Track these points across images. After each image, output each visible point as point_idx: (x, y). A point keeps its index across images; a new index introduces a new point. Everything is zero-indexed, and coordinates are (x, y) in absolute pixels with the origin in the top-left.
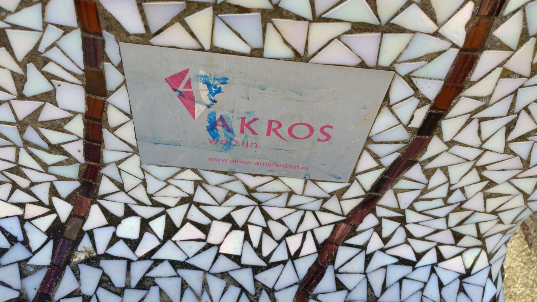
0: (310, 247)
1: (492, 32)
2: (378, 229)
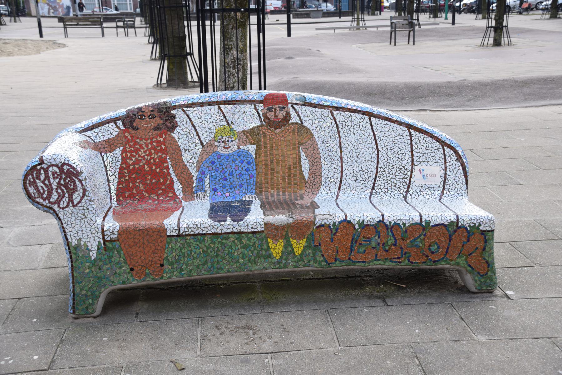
0: (438, 197)
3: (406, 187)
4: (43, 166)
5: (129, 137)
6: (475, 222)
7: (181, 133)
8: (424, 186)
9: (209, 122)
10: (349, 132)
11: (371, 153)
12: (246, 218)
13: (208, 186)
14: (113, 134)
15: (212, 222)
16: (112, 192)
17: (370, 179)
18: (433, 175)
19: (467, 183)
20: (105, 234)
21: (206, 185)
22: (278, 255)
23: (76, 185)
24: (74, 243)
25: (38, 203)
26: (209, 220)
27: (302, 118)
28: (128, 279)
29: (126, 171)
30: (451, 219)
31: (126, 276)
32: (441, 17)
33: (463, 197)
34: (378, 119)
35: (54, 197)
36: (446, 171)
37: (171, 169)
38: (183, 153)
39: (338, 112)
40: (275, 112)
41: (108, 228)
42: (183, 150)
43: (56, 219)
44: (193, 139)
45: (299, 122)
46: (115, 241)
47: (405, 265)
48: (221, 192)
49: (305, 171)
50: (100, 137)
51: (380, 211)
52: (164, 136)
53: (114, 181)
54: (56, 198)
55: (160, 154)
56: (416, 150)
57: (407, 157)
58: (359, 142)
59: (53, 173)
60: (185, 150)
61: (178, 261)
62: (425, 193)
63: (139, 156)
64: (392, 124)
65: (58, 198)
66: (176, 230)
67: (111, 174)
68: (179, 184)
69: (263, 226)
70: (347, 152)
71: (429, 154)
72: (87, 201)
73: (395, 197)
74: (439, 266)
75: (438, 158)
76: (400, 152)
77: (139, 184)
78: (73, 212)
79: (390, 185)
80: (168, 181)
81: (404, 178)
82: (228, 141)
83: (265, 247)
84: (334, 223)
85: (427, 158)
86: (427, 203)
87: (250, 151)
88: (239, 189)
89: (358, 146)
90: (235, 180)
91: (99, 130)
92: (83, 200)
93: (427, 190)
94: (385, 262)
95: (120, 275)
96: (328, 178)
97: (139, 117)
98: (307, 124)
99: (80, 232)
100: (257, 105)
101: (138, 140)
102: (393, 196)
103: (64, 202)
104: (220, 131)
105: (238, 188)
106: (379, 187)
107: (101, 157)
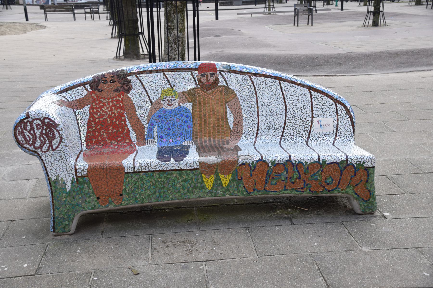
0: (332, 141)
2: (338, 139)
3: (308, 134)
4: (29, 119)
5: (95, 97)
6: (360, 160)
7: (135, 93)
8: (321, 133)
11: (281, 108)
12: (185, 158)
13: (156, 134)
14: (83, 95)
15: (159, 162)
16: (82, 139)
17: (280, 128)
18: (328, 125)
19: (354, 131)
20: (78, 171)
22: (210, 187)
23: (55, 134)
24: (54, 178)
25: (25, 148)
26: (157, 160)
27: (228, 82)
28: (95, 206)
29: (93, 123)
30: (342, 159)
32: (333, 4)
33: (351, 142)
34: (286, 83)
35: (38, 143)
37: (128, 122)
38: (136, 109)
39: (255, 77)
40: (207, 78)
41: (80, 167)
42: (137, 107)
44: (144, 98)
45: (226, 85)
46: (85, 176)
47: (307, 194)
48: (166, 138)
49: (230, 122)
50: (72, 97)
51: (288, 153)
52: (122, 96)
53: (84, 131)
54: (39, 144)
55: (119, 110)
56: (315, 106)
58: (271, 100)
59: (37, 125)
60: (139, 107)
61: (133, 192)
62: (322, 138)
63: (103, 111)
64: (297, 86)
65: (41, 144)
66: (132, 168)
67: (82, 126)
68: (134, 133)
69: (198, 165)
70: (263, 107)
71: (325, 109)
72: (63, 146)
73: (299, 142)
74: (333, 194)
75: (332, 112)
76: (303, 108)
77: (103, 133)
78: (52, 155)
79: (295, 133)
81: (306, 127)
82: (171, 100)
84: (253, 162)
85: (324, 112)
86: (323, 146)
87: (188, 108)
88: (179, 137)
89: (270, 103)
91: (72, 92)
92: (60, 146)
93: (324, 136)
94: (291, 192)
96: (248, 127)
97: (103, 82)
98: (232, 86)
99: (58, 170)
101: (102, 100)
102: (298, 141)
103: (45, 147)
104: (165, 93)
105: (179, 135)
106: (287, 134)
107: (73, 113)
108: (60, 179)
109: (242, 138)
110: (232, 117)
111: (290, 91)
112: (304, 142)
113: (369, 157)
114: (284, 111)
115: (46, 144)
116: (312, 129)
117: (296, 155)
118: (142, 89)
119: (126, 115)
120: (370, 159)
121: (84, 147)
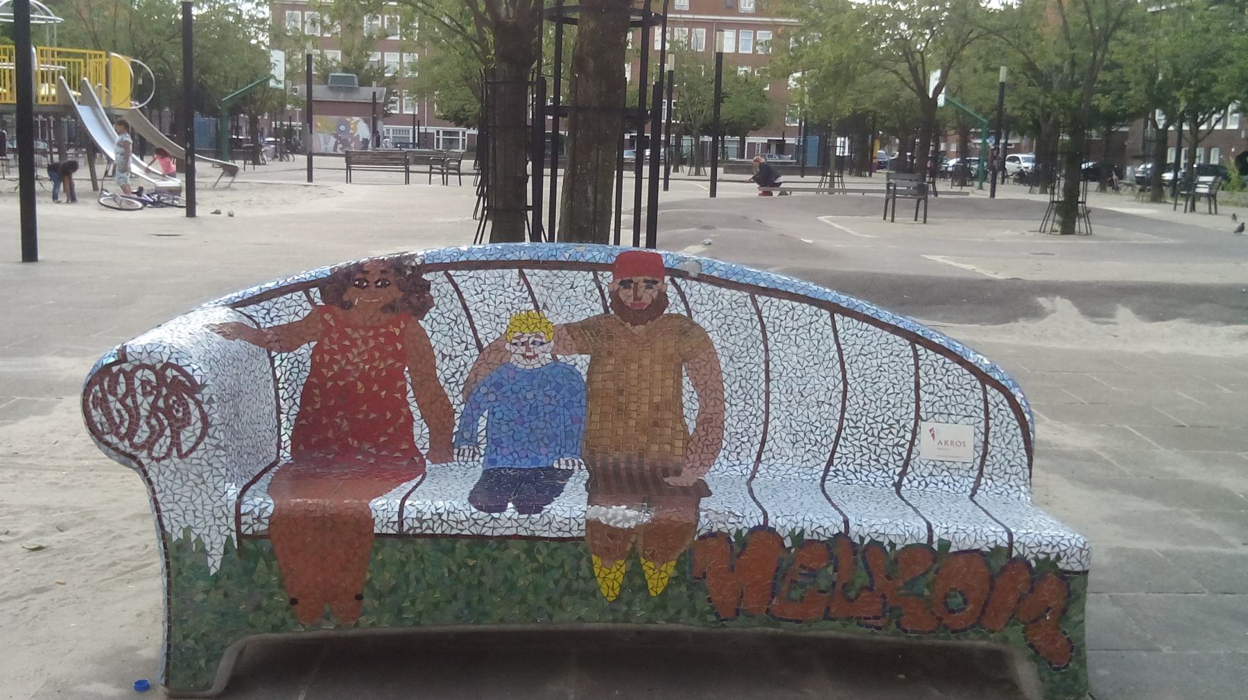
0: (968, 489)
1: (1125, 305)
2: (986, 483)
3: (901, 463)
4: (124, 366)
5: (332, 323)
6: (1048, 550)
7: (438, 319)
8: (938, 464)
9: (498, 302)
10: (787, 342)
11: (831, 388)
12: (548, 507)
13: (484, 433)
14: (300, 314)
15: (474, 510)
16: (283, 432)
17: (824, 442)
18: (958, 444)
19: (1030, 465)
20: (243, 521)
21: (479, 431)
22: (611, 593)
23: (189, 413)
24: (177, 535)
25: (108, 444)
26: (467, 506)
27: (690, 305)
28: (284, 622)
29: (317, 391)
30: (996, 541)
31: (280, 614)
32: (973, 185)
33: (1022, 495)
34: (849, 319)
35: (142, 435)
36: (986, 438)
37: (411, 394)
38: (438, 362)
39: (766, 298)
40: (636, 291)
41: (250, 508)
42: (440, 356)
43: (143, 480)
44: (461, 333)
45: (685, 314)
46: (262, 537)
47: (887, 636)
48: (511, 447)
49: (688, 415)
50: (272, 319)
51: (841, 513)
52: (403, 326)
53: (290, 409)
54: (145, 436)
55: (390, 361)
56: (925, 388)
57: (907, 401)
58: (806, 363)
59: (144, 383)
60: (444, 356)
61: (393, 590)
62: (940, 478)
63: (348, 362)
64: (878, 330)
65: (149, 437)
66: (394, 522)
67: (286, 396)
68: (425, 425)
69: (583, 527)
70: (781, 382)
71: (953, 398)
72: (209, 447)
73: (876, 485)
74: (965, 642)
75: (972, 408)
76: (891, 391)
77: (342, 420)
78: (177, 469)
79: (867, 457)
80: (403, 418)
81: (897, 445)
82: (534, 343)
83: (584, 572)
84: (739, 532)
85: (949, 407)
86: (944, 500)
87: (577, 367)
88: (547, 446)
89: (803, 372)
90: (541, 424)
91: (271, 305)
92: (201, 446)
93: (945, 473)
94: (844, 626)
95: (268, 613)
96: (737, 433)
97: (357, 283)
98: (700, 319)
99: (191, 513)
100: (600, 273)
101: (349, 330)
102: (872, 481)
103: (161, 446)
104: (520, 320)
105: (546, 441)
106: (844, 460)
107: (268, 360)
108: (193, 540)
109: (717, 461)
110: (694, 401)
111: (858, 342)
112: (889, 486)
113: (1073, 542)
114: (840, 396)
115: (164, 437)
116: (914, 450)
117: (864, 520)
118: (460, 310)
119: (408, 376)
120: (1076, 549)
121: (286, 455)
